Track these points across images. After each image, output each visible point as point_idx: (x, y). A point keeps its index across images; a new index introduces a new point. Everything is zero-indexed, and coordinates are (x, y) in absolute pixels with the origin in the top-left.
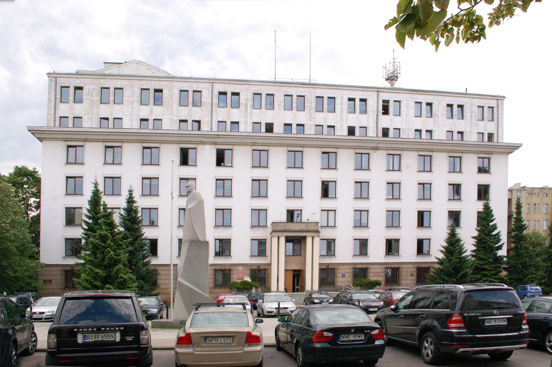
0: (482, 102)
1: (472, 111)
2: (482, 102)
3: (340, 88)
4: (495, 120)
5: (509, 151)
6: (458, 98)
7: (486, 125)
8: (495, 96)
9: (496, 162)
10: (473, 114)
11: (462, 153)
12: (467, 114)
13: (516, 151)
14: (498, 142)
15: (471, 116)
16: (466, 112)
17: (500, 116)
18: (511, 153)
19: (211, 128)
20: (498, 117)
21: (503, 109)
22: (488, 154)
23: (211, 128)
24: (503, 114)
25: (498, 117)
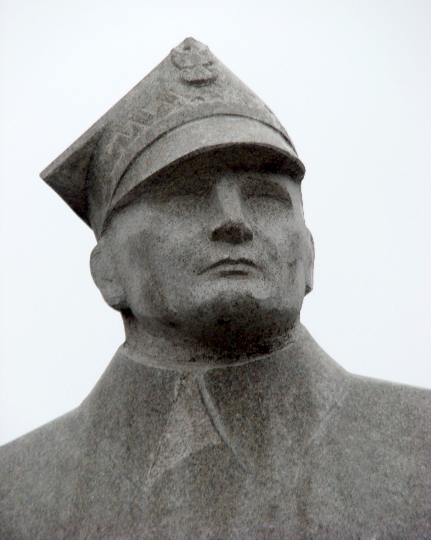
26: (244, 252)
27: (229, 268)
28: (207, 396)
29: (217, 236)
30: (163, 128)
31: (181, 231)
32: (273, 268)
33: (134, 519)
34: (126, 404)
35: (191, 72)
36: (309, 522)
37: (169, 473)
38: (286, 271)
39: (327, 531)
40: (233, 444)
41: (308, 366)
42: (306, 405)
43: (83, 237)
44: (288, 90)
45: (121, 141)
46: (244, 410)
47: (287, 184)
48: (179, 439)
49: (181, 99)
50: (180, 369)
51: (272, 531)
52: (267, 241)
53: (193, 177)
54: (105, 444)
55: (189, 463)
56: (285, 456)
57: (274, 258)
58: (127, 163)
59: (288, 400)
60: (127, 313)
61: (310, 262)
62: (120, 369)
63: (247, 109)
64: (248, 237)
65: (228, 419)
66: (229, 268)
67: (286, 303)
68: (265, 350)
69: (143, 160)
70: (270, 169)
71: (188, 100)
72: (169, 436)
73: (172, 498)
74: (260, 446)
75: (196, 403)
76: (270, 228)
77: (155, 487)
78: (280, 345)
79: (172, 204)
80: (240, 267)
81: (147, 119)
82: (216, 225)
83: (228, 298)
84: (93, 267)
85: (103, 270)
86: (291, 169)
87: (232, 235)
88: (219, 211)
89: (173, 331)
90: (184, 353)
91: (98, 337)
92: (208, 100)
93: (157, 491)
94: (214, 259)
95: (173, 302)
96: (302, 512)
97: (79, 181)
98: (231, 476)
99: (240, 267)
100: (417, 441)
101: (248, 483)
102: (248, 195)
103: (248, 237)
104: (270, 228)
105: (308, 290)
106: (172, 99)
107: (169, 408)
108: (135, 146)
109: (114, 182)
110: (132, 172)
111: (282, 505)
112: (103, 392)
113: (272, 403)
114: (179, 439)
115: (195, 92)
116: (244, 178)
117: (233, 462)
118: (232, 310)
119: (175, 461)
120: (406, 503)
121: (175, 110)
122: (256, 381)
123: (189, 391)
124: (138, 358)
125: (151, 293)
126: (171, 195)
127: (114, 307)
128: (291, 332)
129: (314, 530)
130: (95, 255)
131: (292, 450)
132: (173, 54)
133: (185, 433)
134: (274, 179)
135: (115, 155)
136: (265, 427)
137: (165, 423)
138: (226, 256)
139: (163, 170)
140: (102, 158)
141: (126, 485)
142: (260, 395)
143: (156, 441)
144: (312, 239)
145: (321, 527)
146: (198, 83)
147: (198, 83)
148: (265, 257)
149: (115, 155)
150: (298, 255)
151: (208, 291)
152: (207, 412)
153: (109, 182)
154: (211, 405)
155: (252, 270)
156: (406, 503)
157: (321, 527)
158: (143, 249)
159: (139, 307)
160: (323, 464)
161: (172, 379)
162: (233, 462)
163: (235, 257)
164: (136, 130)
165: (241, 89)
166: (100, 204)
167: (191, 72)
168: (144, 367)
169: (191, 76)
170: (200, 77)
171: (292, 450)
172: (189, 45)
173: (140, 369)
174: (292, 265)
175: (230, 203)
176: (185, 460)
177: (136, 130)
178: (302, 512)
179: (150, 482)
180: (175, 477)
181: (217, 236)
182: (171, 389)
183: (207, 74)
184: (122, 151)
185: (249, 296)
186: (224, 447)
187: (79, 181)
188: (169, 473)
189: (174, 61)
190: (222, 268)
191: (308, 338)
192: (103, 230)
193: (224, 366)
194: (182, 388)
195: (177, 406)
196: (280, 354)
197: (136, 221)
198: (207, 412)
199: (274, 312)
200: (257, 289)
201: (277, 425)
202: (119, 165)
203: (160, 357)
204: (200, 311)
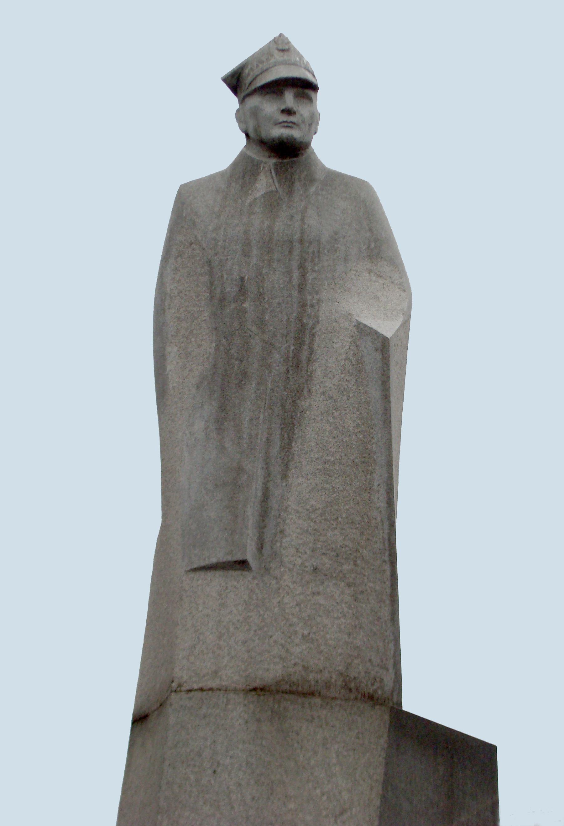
26: (292, 119)
27: (286, 124)
28: (273, 172)
29: (283, 111)
30: (267, 67)
31: (270, 107)
32: (302, 126)
33: (241, 214)
34: (243, 171)
35: (281, 46)
36: (304, 223)
37: (255, 199)
38: (307, 127)
39: (311, 227)
40: (280, 191)
41: (313, 162)
42: (310, 179)
45: (252, 69)
46: (286, 178)
47: (312, 93)
48: (260, 186)
49: (275, 55)
50: (264, 160)
51: (290, 225)
52: (302, 115)
53: (276, 87)
54: (233, 184)
55: (263, 196)
56: (264, 231)
57: (303, 122)
58: (253, 78)
59: (303, 176)
60: (247, 135)
61: (318, 122)
62: (242, 157)
64: (295, 113)
65: (279, 182)
66: (286, 124)
67: (306, 139)
68: (297, 156)
69: (259, 78)
70: (305, 87)
71: (278, 56)
72: (257, 185)
73: (256, 208)
74: (290, 193)
75: (269, 173)
76: (303, 110)
77: (250, 203)
78: (303, 155)
79: (268, 97)
80: (290, 125)
81: (262, 62)
82: (283, 107)
83: (284, 136)
85: (240, 117)
86: (313, 87)
87: (288, 112)
88: (285, 102)
89: (263, 145)
90: (267, 154)
91: (234, 143)
92: (286, 57)
93: (250, 205)
94: (281, 120)
95: (264, 135)
96: (302, 219)
97: (235, 81)
98: (278, 203)
99: (290, 125)
100: (348, 196)
101: (284, 207)
103: (295, 113)
104: (303, 110)
105: (315, 133)
106: (272, 56)
107: (258, 174)
108: (256, 72)
109: (247, 85)
110: (254, 82)
111: (295, 216)
112: (235, 165)
113: (297, 177)
114: (260, 186)
115: (282, 53)
116: (295, 90)
117: (279, 198)
118: (285, 141)
119: (258, 195)
120: (341, 219)
121: (273, 60)
122: (292, 167)
123: (266, 169)
124: (249, 153)
125: (256, 130)
126: (268, 93)
127: (243, 132)
128: (307, 150)
129: (306, 226)
130: (238, 111)
131: (302, 195)
132: (275, 38)
133: (264, 183)
134: (307, 91)
135: (249, 74)
136: (293, 186)
137: (256, 180)
138: (285, 120)
139: (266, 84)
140: (244, 75)
141: (240, 201)
142: (292, 173)
143: (252, 186)
145: (308, 225)
146: (283, 51)
147: (283, 51)
148: (300, 121)
149: (249, 74)
150: (313, 122)
151: (277, 132)
152: (272, 177)
153: (245, 84)
154: (274, 175)
155: (295, 126)
156: (341, 219)
157: (308, 225)
158: (255, 112)
159: (252, 134)
160: (313, 202)
161: (261, 163)
162: (279, 198)
163: (289, 121)
164: (257, 66)
165: (299, 54)
166: (241, 93)
167: (281, 46)
168: (251, 158)
169: (280, 47)
170: (284, 48)
171: (302, 195)
172: (281, 35)
173: (249, 157)
174: (310, 125)
175: (289, 98)
176: (262, 195)
177: (257, 66)
178: (302, 219)
179: (248, 201)
180: (258, 201)
181: (283, 111)
182: (260, 167)
183: (287, 47)
184: (251, 73)
185: (292, 136)
186: (277, 191)
187: (235, 81)
188: (255, 199)
189: (275, 41)
190: (283, 124)
191: (313, 152)
192: (242, 101)
193: (280, 161)
194: (264, 167)
195: (262, 174)
196: (302, 158)
197: (254, 101)
198: (272, 177)
199: (301, 142)
200: (296, 134)
201: (297, 185)
202: (249, 79)
203: (258, 155)
204: (273, 140)
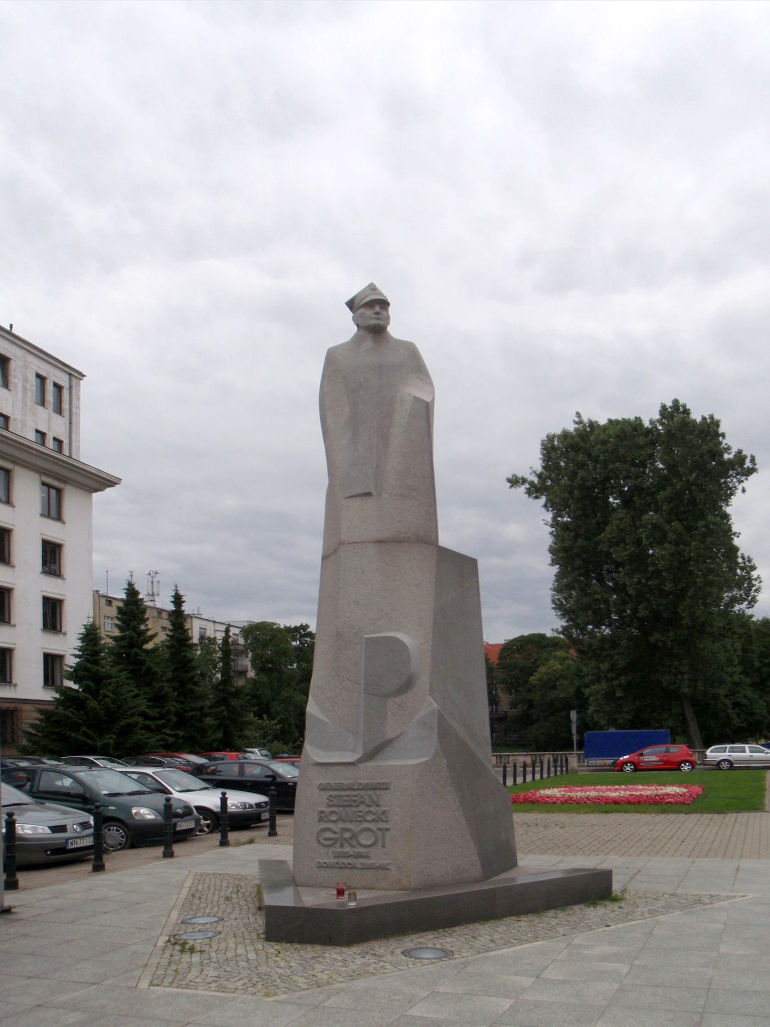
0: (45, 369)
1: (26, 380)
2: (45, 369)
3: (23, 345)
4: (66, 413)
5: (97, 486)
6: (14, 347)
7: (50, 419)
8: (68, 366)
9: (72, 500)
10: (28, 386)
11: (14, 462)
12: (16, 381)
13: (108, 490)
14: (70, 457)
15: (24, 388)
16: (15, 377)
17: (74, 410)
18: (96, 490)
19: (383, 834)
20: (70, 410)
21: (79, 399)
22: (59, 480)
23: (383, 834)
24: (78, 408)
25: (70, 410)
31: (368, 312)
34: (356, 340)
35: (372, 288)
43: (350, 314)
44: (387, 293)
53: (371, 304)
60: (358, 326)
63: (381, 294)
76: (384, 313)
84: (298, 727)
85: (354, 319)
86: (388, 304)
87: (378, 313)
97: (351, 304)
102: (381, 308)
144: (607, 812)
151: (373, 322)
167: (372, 288)
187: (351, 304)
189: (369, 286)
200: (381, 322)
